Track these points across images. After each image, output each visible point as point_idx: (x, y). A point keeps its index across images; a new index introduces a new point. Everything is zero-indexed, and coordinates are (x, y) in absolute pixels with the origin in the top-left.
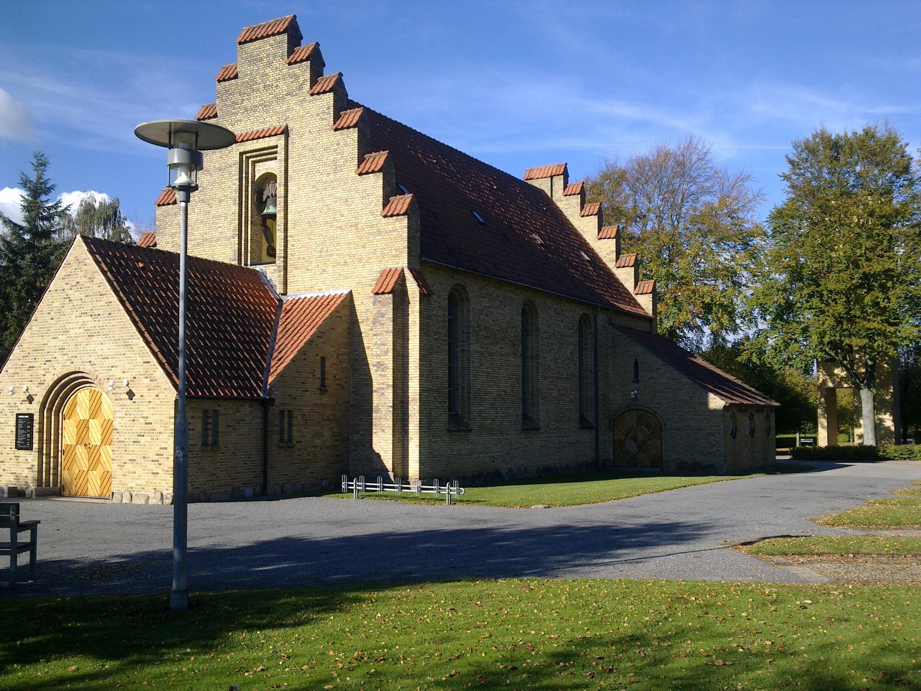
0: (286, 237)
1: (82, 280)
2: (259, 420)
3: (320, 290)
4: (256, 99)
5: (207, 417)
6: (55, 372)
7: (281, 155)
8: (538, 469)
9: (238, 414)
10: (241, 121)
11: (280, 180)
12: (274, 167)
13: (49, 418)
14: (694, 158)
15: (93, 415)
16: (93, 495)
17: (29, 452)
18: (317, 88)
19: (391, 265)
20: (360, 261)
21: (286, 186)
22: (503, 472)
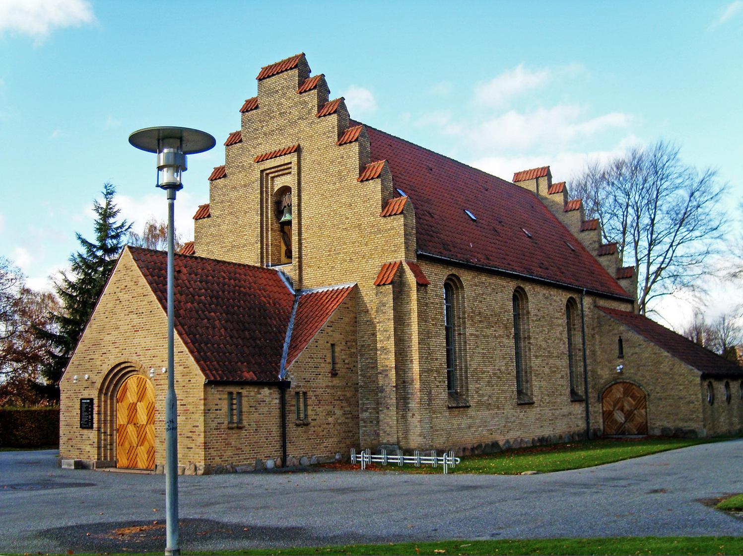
0: (300, 240)
1: (130, 284)
2: (277, 401)
3: (329, 285)
4: (274, 124)
5: (232, 399)
6: (109, 363)
7: (294, 170)
8: (533, 440)
9: (259, 396)
10: (261, 144)
11: (294, 191)
12: (289, 180)
13: (105, 402)
14: (665, 158)
15: (140, 399)
16: (141, 467)
17: (90, 431)
18: (325, 111)
19: (390, 260)
20: (364, 257)
21: (299, 196)
22: (501, 443)
